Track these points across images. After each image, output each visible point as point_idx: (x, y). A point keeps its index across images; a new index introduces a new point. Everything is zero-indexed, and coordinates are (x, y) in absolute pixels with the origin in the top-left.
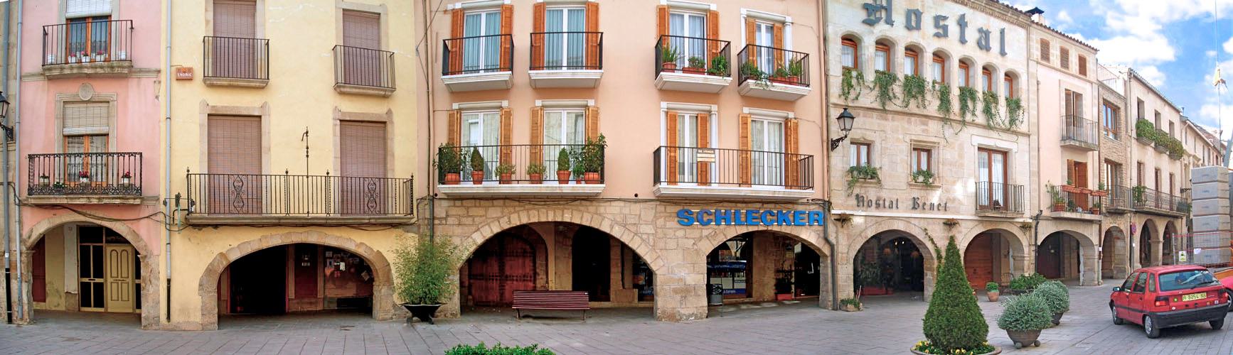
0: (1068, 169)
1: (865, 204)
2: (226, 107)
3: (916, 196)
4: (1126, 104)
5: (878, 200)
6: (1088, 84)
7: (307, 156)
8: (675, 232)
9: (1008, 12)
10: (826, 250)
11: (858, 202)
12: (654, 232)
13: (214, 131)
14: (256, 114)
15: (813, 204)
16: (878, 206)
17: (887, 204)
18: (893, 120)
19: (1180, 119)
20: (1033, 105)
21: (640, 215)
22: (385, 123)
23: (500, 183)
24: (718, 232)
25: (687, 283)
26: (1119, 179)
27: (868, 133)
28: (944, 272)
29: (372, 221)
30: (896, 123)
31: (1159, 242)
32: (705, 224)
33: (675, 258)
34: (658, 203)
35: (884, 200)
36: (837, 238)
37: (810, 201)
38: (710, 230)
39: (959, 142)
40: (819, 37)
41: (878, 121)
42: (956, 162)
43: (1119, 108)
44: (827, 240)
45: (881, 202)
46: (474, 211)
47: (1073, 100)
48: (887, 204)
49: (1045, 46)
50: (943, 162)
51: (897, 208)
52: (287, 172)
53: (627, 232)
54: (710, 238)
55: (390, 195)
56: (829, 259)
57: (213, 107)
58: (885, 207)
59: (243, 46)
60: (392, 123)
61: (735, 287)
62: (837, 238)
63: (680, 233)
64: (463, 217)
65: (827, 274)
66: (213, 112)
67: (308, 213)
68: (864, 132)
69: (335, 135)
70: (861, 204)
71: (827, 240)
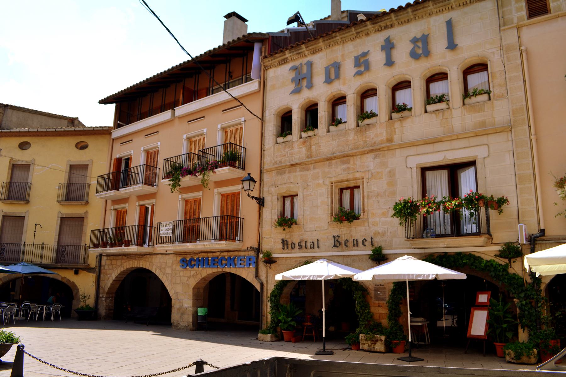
1: (290, 246)
2: (10, 212)
3: (336, 234)
7: (35, 235)
11: (283, 246)
12: (171, 273)
13: (5, 223)
14: (23, 216)
16: (300, 247)
17: (309, 244)
18: (314, 168)
21: (166, 263)
22: (84, 218)
24: (198, 273)
27: (292, 186)
29: (63, 266)
30: (317, 170)
32: (192, 266)
33: (179, 289)
34: (174, 255)
35: (306, 242)
36: (267, 277)
37: (249, 249)
38: (194, 272)
39: (388, 170)
41: (301, 173)
42: (385, 192)
45: (303, 244)
46: (114, 262)
48: (309, 244)
50: (368, 195)
51: (318, 247)
52: (43, 243)
53: (161, 272)
54: (194, 277)
55: (81, 254)
57: (5, 212)
58: (306, 248)
59: (23, 185)
60: (87, 217)
62: (267, 277)
63: (182, 274)
66: (4, 215)
67: (32, 261)
68: (288, 185)
69: (57, 225)
70: (286, 247)
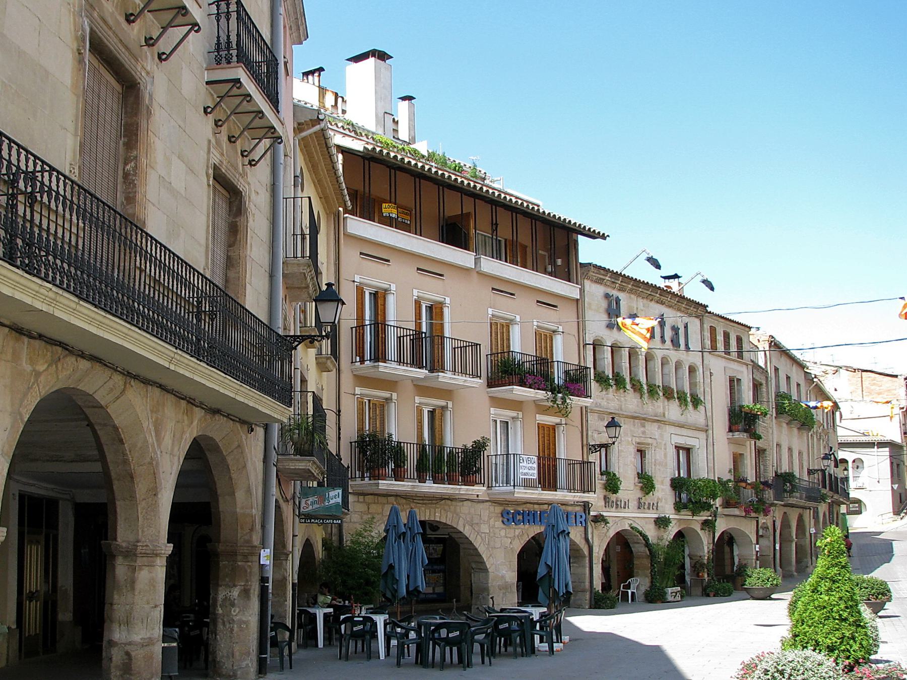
0: (734, 462)
4: (767, 378)
5: (617, 501)
6: (744, 366)
8: (500, 531)
9: (691, 306)
10: (586, 552)
11: (605, 504)
12: (488, 532)
15: (577, 505)
19: (805, 377)
20: (708, 397)
23: (370, 480)
25: (507, 580)
26: (762, 467)
28: (822, 567)
31: (791, 541)
35: (621, 501)
40: (579, 345)
43: (761, 384)
44: (587, 540)
47: (734, 383)
49: (713, 330)
56: (587, 559)
61: (436, 592)
64: (365, 514)
65: (585, 574)
71: (587, 540)
